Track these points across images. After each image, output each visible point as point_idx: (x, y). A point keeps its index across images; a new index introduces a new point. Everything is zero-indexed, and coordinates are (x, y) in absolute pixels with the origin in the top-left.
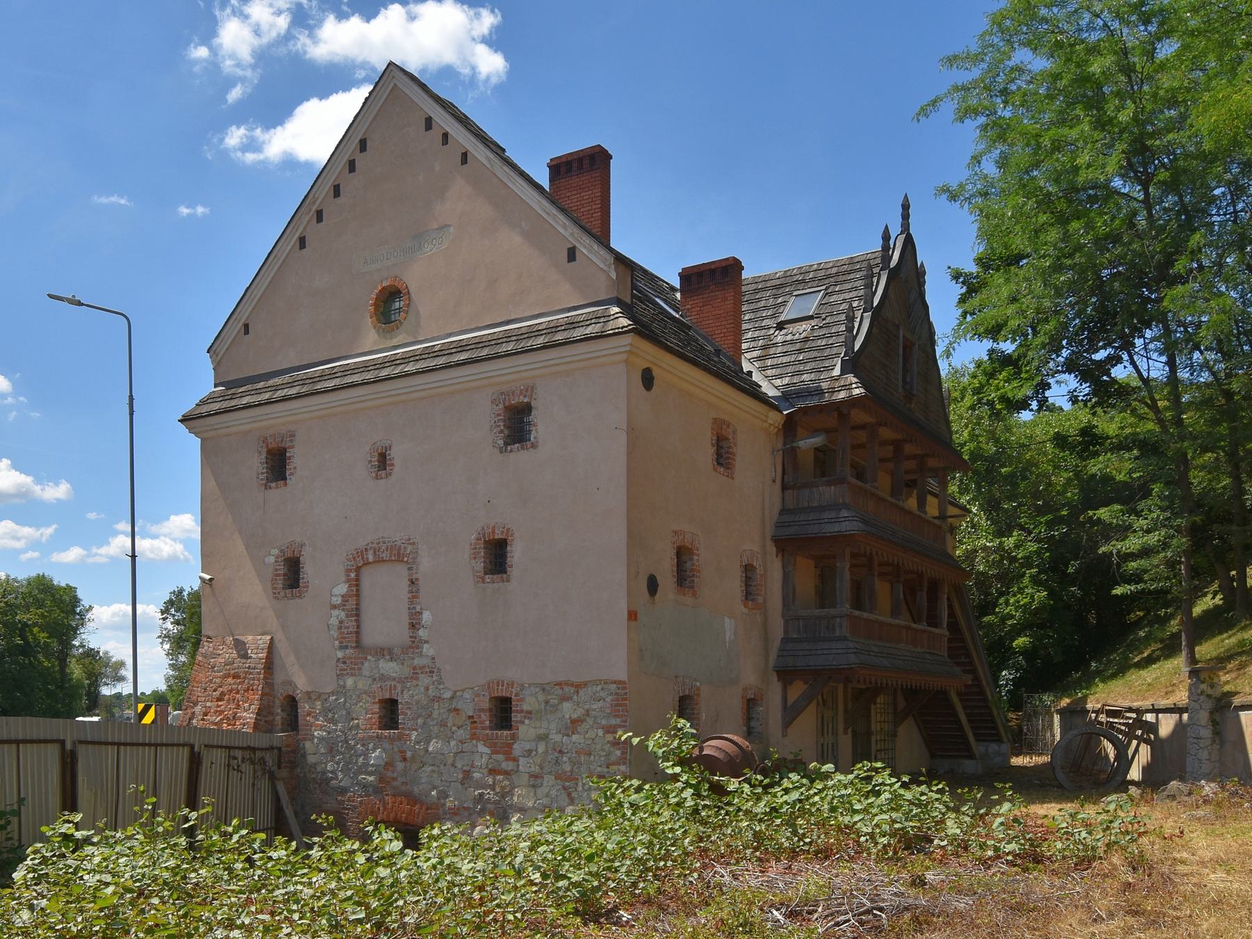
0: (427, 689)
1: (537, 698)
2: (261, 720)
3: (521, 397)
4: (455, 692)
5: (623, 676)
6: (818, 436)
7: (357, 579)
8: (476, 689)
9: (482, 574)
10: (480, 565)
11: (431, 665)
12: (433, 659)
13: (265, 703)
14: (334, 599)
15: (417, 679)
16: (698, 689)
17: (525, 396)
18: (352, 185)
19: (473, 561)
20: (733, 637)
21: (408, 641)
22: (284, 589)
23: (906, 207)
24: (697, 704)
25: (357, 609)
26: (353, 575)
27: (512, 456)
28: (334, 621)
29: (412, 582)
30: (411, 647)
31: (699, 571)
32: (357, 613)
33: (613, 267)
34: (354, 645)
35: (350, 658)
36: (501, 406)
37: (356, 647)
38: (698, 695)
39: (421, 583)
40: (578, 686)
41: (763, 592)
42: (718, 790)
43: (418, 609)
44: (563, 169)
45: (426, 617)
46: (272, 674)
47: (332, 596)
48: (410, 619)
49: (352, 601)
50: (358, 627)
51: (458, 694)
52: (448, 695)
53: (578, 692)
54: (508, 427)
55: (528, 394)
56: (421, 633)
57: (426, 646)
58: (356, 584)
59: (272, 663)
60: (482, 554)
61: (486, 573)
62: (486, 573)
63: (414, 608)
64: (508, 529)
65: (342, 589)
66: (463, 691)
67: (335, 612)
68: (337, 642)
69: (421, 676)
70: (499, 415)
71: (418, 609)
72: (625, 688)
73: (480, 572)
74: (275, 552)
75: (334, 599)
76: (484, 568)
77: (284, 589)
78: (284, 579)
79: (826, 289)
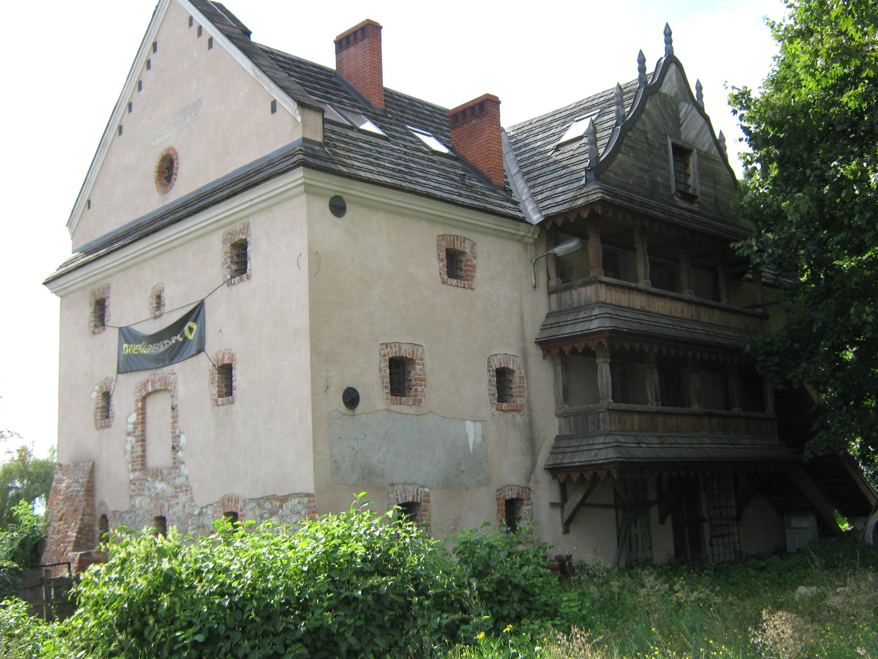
0: (184, 506)
1: (254, 513)
2: (81, 538)
3: (241, 235)
4: (202, 508)
5: (311, 490)
6: (572, 241)
7: (143, 408)
8: (215, 505)
9: (216, 397)
10: (215, 391)
11: (186, 483)
12: (187, 478)
13: (86, 522)
14: (129, 426)
15: (177, 497)
16: (428, 495)
17: (243, 234)
18: (149, 78)
19: (211, 386)
20: (479, 440)
21: (170, 462)
22: (101, 419)
23: (668, 33)
24: (426, 510)
25: (142, 435)
26: (140, 405)
27: (234, 287)
28: (128, 447)
29: (173, 409)
30: (173, 468)
31: (424, 380)
32: (142, 440)
33: (297, 112)
34: (140, 467)
35: (138, 480)
36: (229, 245)
37: (142, 469)
38: (428, 501)
39: (179, 408)
40: (284, 499)
41: (526, 394)
42: (391, 606)
43: (177, 433)
44: (344, 43)
45: (183, 439)
46: (93, 496)
47: (128, 424)
48: (173, 442)
49: (140, 428)
50: (144, 451)
51: (204, 510)
52: (196, 512)
53: (282, 506)
54: (237, 263)
55: (245, 231)
56: (180, 454)
57: (183, 466)
58: (142, 412)
59: (93, 486)
60: (217, 379)
61: (220, 396)
62: (220, 396)
63: (175, 432)
64: (232, 355)
65: (133, 418)
66: (206, 507)
67: (129, 439)
68: (130, 466)
69: (181, 494)
70: (227, 253)
71: (177, 433)
72: (314, 501)
73: (215, 395)
74: (97, 388)
75: (129, 426)
76: (218, 391)
77: (101, 419)
78: (102, 412)
79: (599, 112)
